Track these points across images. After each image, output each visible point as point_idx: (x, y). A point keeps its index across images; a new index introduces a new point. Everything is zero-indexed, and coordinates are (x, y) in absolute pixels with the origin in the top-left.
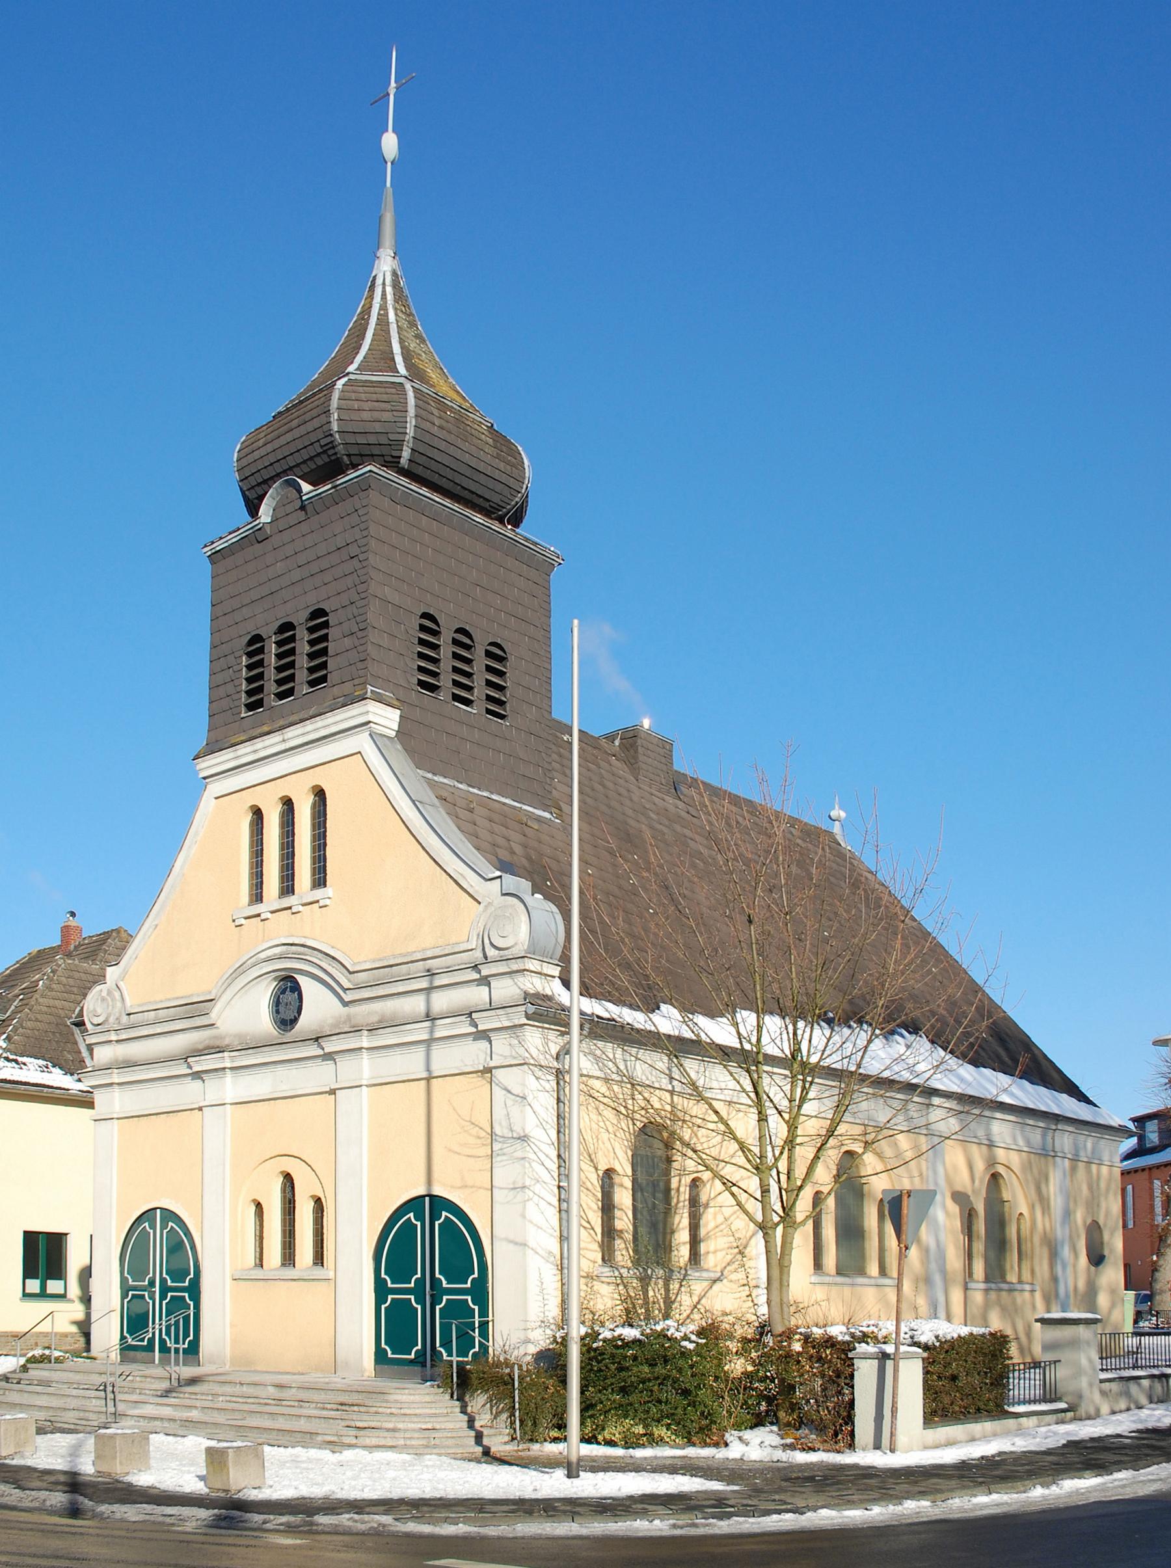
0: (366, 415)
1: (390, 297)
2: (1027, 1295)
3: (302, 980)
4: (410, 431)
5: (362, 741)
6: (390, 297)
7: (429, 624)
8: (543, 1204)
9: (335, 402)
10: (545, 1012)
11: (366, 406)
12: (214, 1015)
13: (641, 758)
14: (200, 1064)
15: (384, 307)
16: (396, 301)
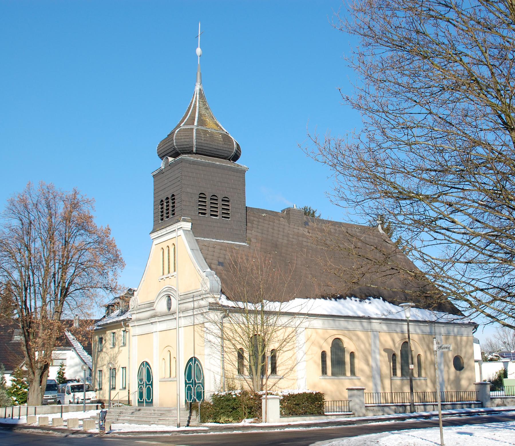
0: (183, 140)
1: (198, 98)
2: (423, 381)
3: (171, 297)
4: (195, 143)
5: (181, 232)
6: (198, 98)
7: (202, 196)
8: (216, 359)
9: (174, 138)
10: (214, 307)
11: (183, 137)
12: (154, 306)
13: (291, 217)
14: (153, 320)
15: (196, 102)
16: (200, 99)
